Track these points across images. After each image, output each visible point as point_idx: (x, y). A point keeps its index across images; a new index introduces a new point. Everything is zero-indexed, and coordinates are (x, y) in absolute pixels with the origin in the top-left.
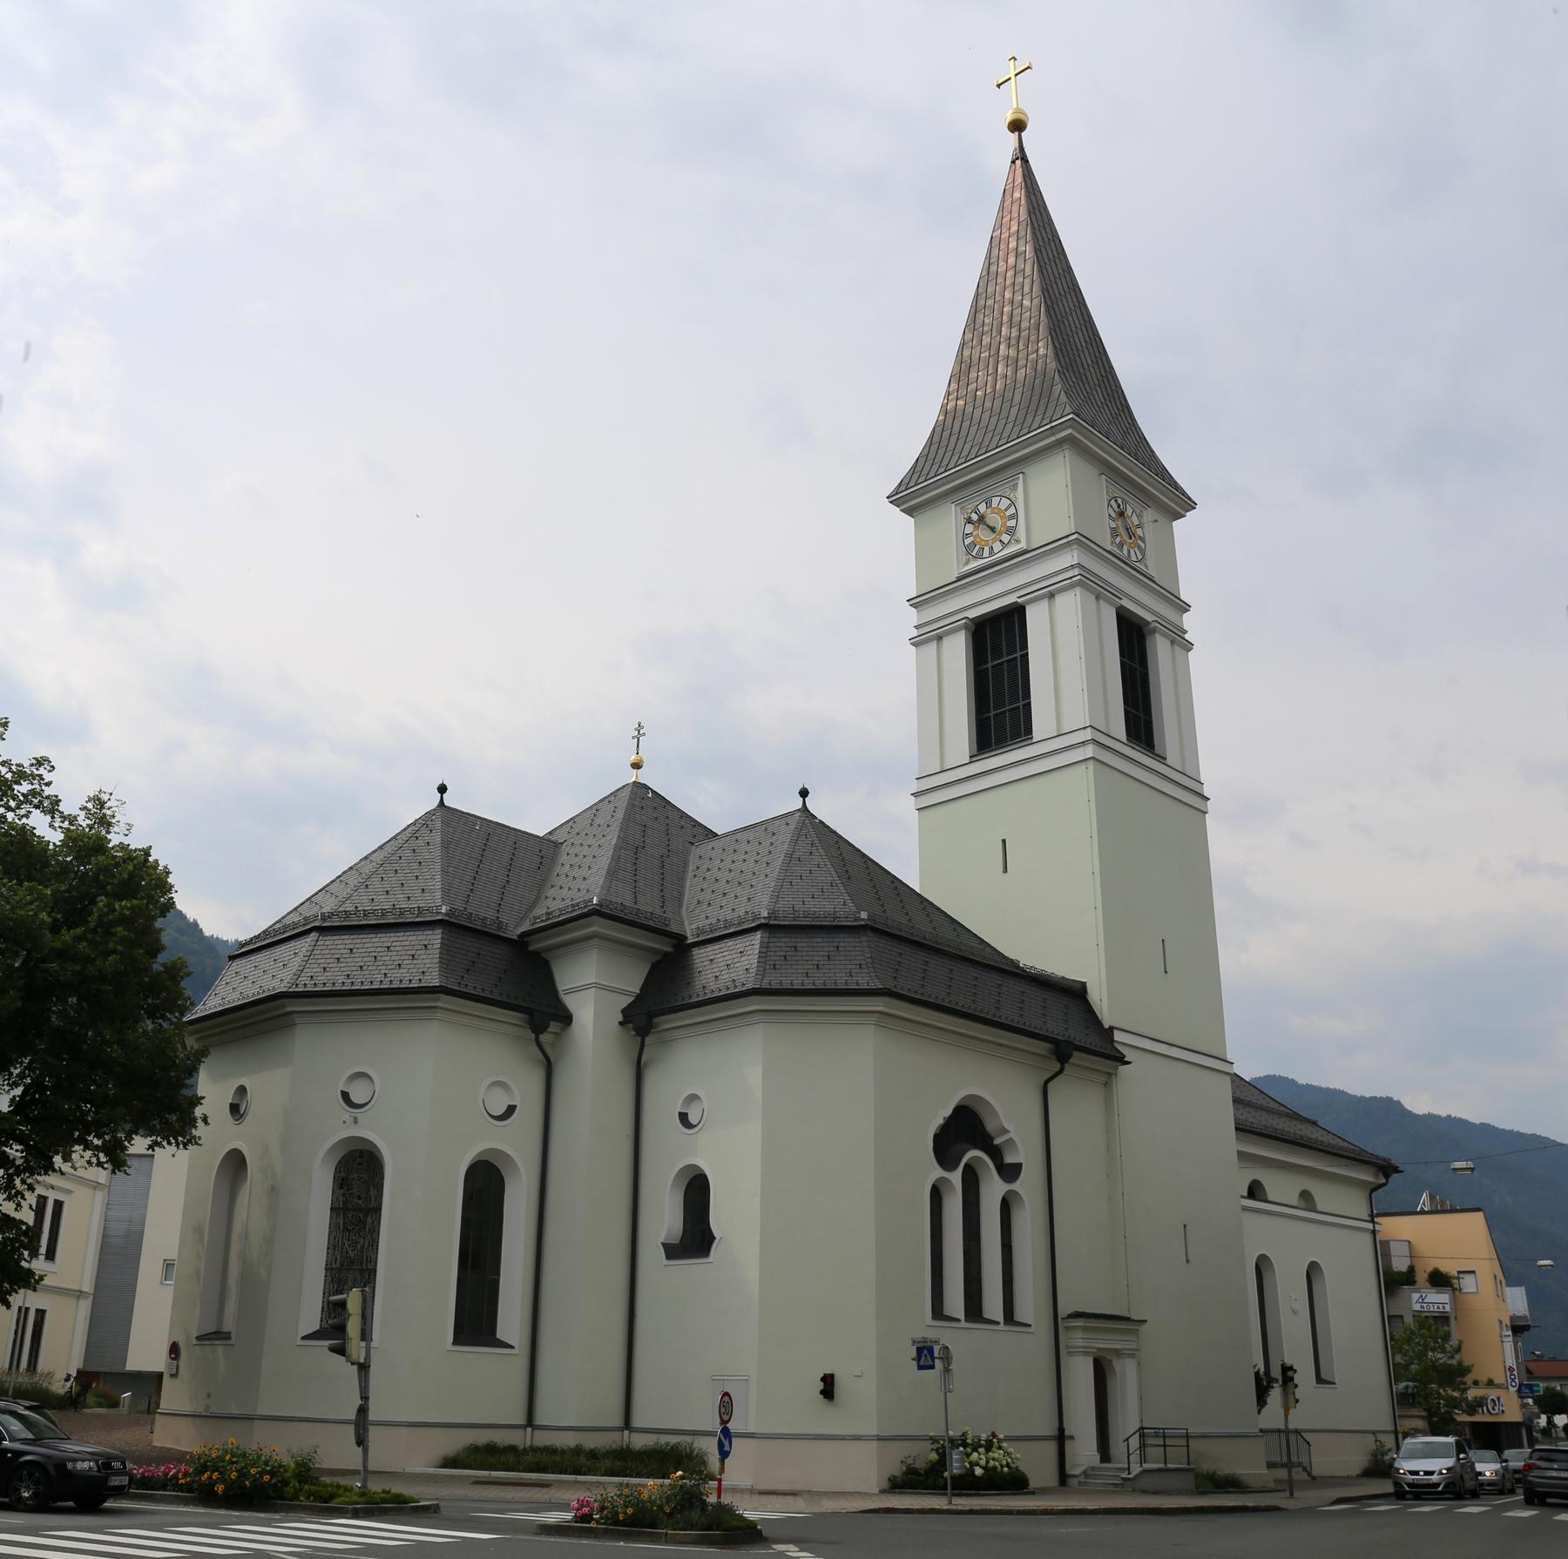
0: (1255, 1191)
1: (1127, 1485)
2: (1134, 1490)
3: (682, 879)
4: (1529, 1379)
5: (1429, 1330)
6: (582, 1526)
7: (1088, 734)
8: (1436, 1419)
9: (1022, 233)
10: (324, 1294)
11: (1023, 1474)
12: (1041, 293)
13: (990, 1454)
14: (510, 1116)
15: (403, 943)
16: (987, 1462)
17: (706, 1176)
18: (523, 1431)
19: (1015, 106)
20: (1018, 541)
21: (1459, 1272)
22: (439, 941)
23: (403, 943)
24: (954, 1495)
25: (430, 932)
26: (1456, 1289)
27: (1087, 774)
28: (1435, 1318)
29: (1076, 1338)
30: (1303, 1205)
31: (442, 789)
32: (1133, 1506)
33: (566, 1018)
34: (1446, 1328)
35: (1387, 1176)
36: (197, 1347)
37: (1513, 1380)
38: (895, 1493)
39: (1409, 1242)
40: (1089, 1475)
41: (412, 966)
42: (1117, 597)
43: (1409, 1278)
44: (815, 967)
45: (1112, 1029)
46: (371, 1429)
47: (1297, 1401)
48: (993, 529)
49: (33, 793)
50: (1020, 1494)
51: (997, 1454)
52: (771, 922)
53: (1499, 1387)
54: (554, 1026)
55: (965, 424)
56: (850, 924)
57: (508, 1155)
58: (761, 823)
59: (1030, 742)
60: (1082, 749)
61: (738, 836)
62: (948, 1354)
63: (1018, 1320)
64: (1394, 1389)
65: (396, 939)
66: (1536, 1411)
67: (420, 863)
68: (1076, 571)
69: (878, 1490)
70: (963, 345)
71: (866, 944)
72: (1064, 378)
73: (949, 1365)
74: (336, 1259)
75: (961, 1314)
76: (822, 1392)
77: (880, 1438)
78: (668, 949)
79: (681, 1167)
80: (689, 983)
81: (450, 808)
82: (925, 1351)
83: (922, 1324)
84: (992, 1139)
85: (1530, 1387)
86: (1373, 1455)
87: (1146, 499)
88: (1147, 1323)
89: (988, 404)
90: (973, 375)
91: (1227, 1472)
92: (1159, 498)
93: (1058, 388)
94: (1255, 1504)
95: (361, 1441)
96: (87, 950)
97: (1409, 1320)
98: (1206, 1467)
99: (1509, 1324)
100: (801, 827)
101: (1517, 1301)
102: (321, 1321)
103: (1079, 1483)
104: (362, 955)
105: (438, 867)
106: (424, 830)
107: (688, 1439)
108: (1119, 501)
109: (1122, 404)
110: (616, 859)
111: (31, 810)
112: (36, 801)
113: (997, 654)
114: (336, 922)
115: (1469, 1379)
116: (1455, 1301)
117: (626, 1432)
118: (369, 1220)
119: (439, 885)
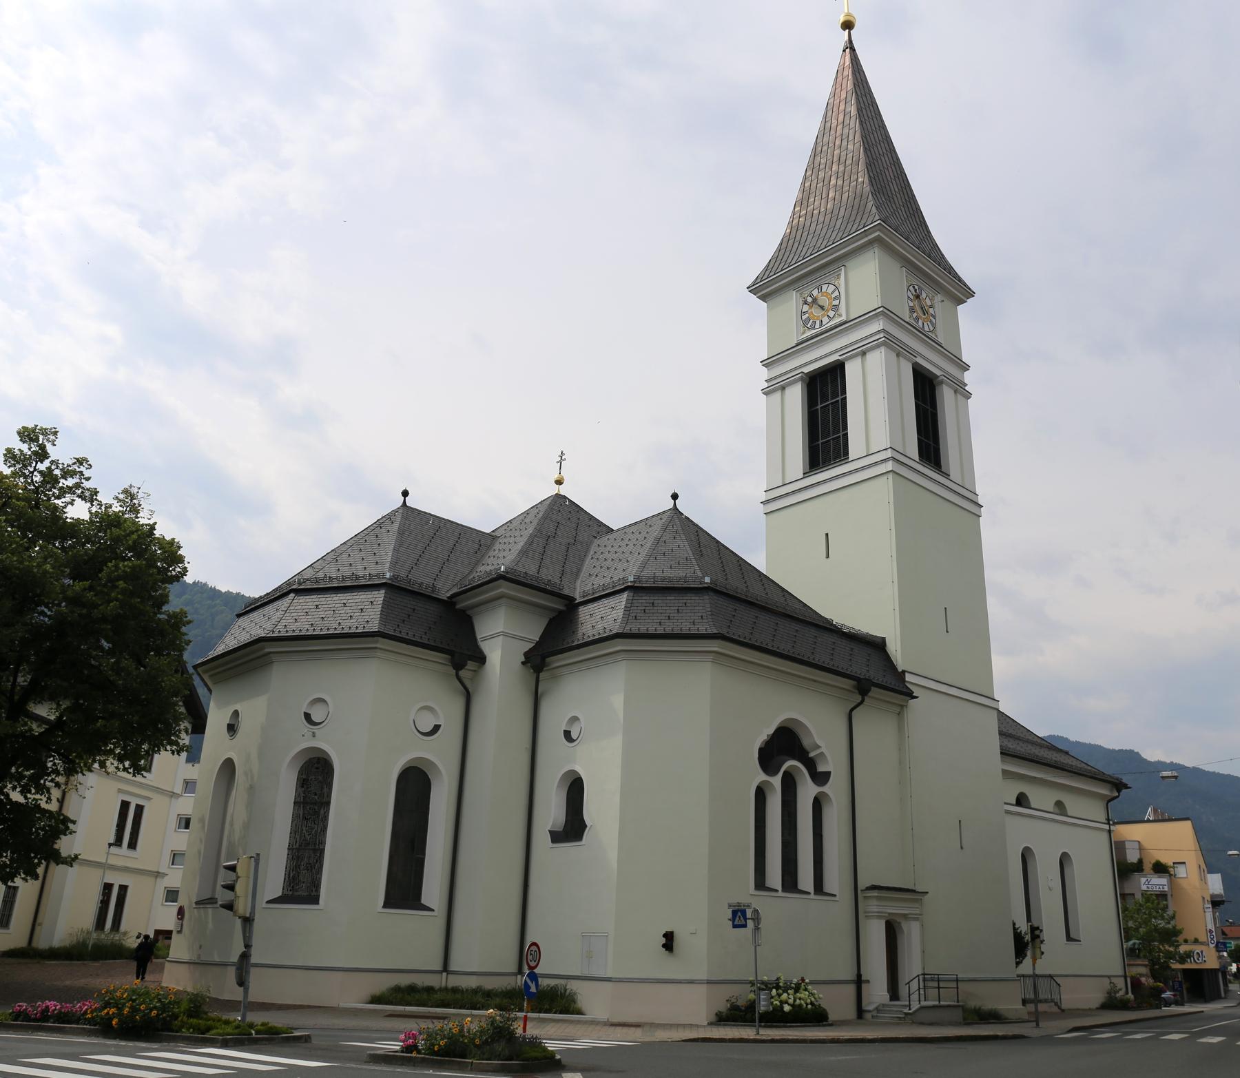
0: (1021, 800)
1: (909, 1018)
2: (913, 1022)
3: (582, 560)
4: (1224, 939)
5: (1153, 903)
6: (409, 1056)
7: (889, 454)
8: (1157, 967)
9: (849, 99)
10: (286, 868)
11: (824, 1010)
12: (861, 139)
13: (798, 994)
14: (433, 735)
15: (357, 601)
16: (795, 1001)
17: (581, 778)
18: (514, 977)
19: (846, 11)
20: (840, 315)
21: (1174, 863)
22: (382, 598)
23: (357, 601)
24: (760, 1026)
25: (377, 592)
26: (1172, 875)
27: (887, 484)
28: (1157, 895)
29: (872, 905)
30: (1057, 810)
31: (405, 494)
32: (904, 1036)
33: (481, 659)
34: (1165, 902)
35: (1119, 791)
36: (195, 910)
37: (1212, 939)
38: (720, 1025)
39: (1139, 842)
40: (880, 1010)
41: (361, 617)
42: (913, 355)
43: (1138, 867)
44: (667, 618)
45: (904, 672)
46: (253, 971)
47: (1043, 953)
48: (822, 308)
49: (77, 486)
50: (819, 1026)
51: (803, 994)
52: (636, 585)
53: (1202, 943)
54: (471, 665)
55: (805, 234)
56: (696, 586)
57: (432, 763)
58: (643, 520)
59: (847, 461)
60: (884, 464)
61: (627, 530)
62: (758, 916)
63: (826, 891)
64: (1125, 947)
65: (351, 597)
66: (1229, 960)
67: (379, 544)
68: (882, 335)
69: (706, 1023)
70: (805, 179)
71: (707, 601)
72: (876, 198)
73: (759, 924)
74: (296, 842)
75: (779, 886)
76: (664, 946)
77: (709, 982)
78: (561, 607)
79: (563, 773)
80: (573, 632)
81: (411, 508)
82: (739, 914)
83: (745, 891)
84: (808, 753)
85: (1224, 944)
86: (1108, 993)
87: (937, 287)
88: (928, 894)
89: (821, 219)
90: (811, 200)
91: (990, 1007)
92: (946, 286)
93: (870, 204)
94: (1005, 1034)
95: (242, 982)
96: (94, 598)
97: (1138, 896)
98: (973, 1003)
99: (1209, 900)
100: (671, 519)
101: (1215, 884)
102: (283, 889)
103: (872, 1016)
104: (325, 609)
105: (392, 547)
106: (388, 522)
107: (563, 982)
108: (916, 287)
109: (920, 221)
110: (530, 542)
111: (74, 498)
112: (79, 492)
113: (825, 398)
114: (308, 585)
115: (1180, 938)
116: (1171, 883)
117: (444, 974)
118: (322, 812)
119: (389, 560)
